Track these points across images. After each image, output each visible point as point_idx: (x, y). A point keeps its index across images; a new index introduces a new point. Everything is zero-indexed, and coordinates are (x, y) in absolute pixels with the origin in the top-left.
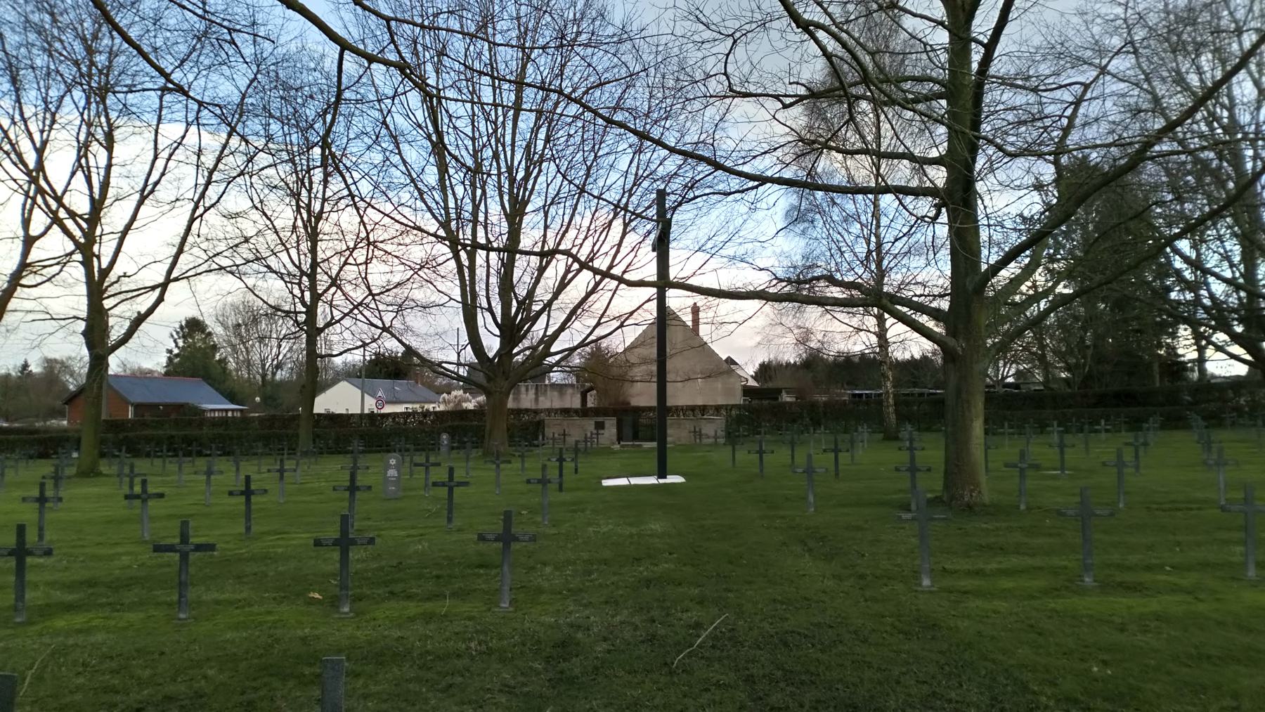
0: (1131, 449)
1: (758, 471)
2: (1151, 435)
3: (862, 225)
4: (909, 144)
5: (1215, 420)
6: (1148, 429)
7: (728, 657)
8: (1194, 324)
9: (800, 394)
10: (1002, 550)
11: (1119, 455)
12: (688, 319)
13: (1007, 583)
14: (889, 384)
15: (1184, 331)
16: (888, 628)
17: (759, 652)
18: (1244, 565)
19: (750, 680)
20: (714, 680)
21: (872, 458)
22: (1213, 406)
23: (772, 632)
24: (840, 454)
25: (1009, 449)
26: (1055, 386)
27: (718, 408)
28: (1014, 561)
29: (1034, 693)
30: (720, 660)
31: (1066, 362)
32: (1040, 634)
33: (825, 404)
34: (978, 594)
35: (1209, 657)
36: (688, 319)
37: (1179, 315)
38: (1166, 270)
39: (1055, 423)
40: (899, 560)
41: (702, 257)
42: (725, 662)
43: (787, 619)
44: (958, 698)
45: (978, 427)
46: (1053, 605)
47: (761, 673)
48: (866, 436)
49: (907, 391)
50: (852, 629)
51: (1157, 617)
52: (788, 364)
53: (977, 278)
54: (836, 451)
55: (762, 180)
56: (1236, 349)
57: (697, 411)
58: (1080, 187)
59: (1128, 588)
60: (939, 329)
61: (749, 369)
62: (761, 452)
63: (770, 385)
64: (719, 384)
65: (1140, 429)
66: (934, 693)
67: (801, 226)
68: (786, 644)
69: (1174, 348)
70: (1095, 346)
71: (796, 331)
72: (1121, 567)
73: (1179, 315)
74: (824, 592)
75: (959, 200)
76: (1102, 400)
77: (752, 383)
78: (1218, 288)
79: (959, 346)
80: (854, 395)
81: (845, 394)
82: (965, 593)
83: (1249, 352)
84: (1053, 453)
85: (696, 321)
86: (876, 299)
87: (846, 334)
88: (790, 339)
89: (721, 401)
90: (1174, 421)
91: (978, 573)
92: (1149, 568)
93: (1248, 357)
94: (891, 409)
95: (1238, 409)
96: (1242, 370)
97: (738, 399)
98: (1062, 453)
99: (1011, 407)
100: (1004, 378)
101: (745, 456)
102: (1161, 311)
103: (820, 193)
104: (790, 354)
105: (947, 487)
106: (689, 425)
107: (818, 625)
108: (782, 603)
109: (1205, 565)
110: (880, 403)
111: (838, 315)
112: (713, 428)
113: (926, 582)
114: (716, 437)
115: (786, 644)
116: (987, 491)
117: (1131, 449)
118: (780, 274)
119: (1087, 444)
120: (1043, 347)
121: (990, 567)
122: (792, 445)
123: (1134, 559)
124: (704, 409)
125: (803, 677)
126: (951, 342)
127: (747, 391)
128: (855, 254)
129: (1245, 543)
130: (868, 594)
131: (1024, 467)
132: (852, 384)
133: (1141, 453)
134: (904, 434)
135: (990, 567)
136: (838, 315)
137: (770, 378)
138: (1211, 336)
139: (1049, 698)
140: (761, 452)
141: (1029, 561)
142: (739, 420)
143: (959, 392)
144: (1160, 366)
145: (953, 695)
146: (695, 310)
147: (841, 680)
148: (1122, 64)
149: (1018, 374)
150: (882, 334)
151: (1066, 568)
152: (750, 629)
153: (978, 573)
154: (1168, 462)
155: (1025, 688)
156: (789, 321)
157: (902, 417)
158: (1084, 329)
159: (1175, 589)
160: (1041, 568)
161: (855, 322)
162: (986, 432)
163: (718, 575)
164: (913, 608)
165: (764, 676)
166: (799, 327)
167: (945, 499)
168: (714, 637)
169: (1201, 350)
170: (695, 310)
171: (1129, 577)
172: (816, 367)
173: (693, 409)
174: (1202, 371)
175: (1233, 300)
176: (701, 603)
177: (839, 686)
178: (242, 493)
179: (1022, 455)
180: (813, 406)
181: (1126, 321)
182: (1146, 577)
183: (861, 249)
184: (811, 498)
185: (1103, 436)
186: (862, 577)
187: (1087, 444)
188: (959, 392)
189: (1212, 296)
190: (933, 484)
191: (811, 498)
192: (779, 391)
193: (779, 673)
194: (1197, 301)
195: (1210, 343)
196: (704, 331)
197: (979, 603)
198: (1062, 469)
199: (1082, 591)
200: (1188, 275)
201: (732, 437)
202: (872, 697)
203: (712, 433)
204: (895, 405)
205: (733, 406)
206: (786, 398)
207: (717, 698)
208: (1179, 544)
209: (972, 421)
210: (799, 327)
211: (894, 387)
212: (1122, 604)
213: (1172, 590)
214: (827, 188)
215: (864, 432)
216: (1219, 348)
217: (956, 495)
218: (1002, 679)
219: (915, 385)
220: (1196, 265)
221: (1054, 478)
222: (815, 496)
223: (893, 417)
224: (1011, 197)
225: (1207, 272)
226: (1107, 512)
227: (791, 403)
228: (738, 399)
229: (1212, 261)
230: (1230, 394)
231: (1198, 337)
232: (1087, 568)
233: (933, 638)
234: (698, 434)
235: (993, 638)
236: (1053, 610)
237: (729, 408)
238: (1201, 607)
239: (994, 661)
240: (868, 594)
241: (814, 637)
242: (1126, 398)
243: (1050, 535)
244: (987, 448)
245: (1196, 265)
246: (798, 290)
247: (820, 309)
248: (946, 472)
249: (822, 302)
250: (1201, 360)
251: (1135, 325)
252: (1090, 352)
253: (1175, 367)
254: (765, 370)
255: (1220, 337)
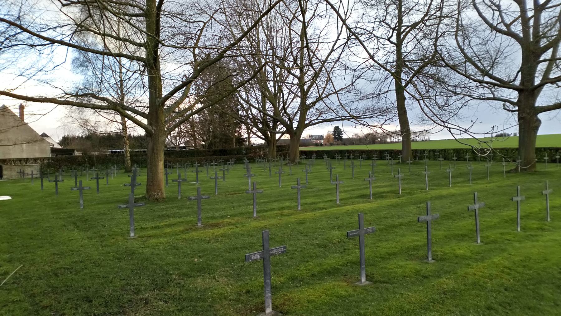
0: (222, 172)
1: (54, 190)
2: (231, 166)
3: (113, 71)
4: (465, 48)
5: (252, 160)
6: (229, 164)
7: (22, 287)
8: (246, 124)
9: (84, 152)
10: (169, 216)
11: (216, 174)
12: (16, 112)
13: (168, 230)
14: (127, 147)
15: (243, 126)
16: (111, 258)
17: (40, 281)
18: (253, 212)
19: (33, 296)
20: (11, 300)
21: (116, 181)
22: (251, 155)
23: (49, 269)
24: (100, 180)
25: (174, 174)
26: (198, 148)
27: (35, 160)
28: (172, 220)
29: (171, 274)
30: (16, 289)
31: (203, 138)
32: (177, 249)
33: (97, 157)
34: (155, 236)
35: (237, 248)
36: (16, 112)
37: (242, 121)
38: (237, 103)
39: (197, 163)
40: (122, 227)
41: (23, 79)
42: (20, 289)
43: (59, 262)
44: (138, 283)
45: (161, 165)
46: (184, 237)
47: (40, 291)
48: (116, 171)
49: (137, 150)
50: (92, 261)
51: (222, 236)
52: (78, 137)
53: (160, 100)
54: (97, 179)
55: (53, 41)
56: (259, 134)
57: (23, 161)
58: (203, 67)
59: (214, 226)
60: (145, 121)
61: (55, 140)
62: (56, 181)
63: (69, 147)
64: (37, 147)
65: (226, 164)
66: (127, 283)
67: (81, 68)
68: (56, 275)
69: (240, 133)
70: (213, 132)
71: (80, 121)
72: (213, 218)
73: (242, 121)
74: (82, 246)
75: (152, 64)
76: (215, 153)
77: (57, 146)
78: (254, 111)
79: (153, 130)
80: (112, 152)
81: (108, 152)
82: (149, 237)
83: (263, 135)
84: (194, 175)
85: (22, 114)
86: (119, 107)
87: (107, 123)
88: (76, 124)
89: (38, 155)
90: (239, 161)
91: (157, 227)
92: (222, 217)
93: (263, 137)
94: (128, 158)
95: (260, 156)
96: (263, 142)
97: (49, 155)
98: (197, 175)
99: (176, 157)
100: (179, 144)
101: (49, 184)
102: (236, 119)
103: (91, 53)
104: (79, 132)
105: (147, 192)
106: (17, 169)
107: (76, 262)
108: (58, 255)
109: (241, 214)
110: (123, 155)
111: (101, 114)
112: (33, 170)
113: (132, 234)
114: (32, 174)
115: (56, 275)
116: (165, 191)
117: (222, 172)
118: (69, 92)
119: (207, 170)
120: (194, 131)
121: (161, 224)
122: (76, 177)
123: (217, 214)
124: (27, 160)
125: (63, 289)
126: (150, 128)
127: (54, 150)
128: (109, 84)
129: (253, 205)
130: (104, 243)
131: (181, 181)
132: (112, 147)
133: (226, 173)
134: (133, 169)
135: (161, 224)
136: (101, 114)
137: (68, 144)
138: (252, 128)
139: (176, 275)
140: (56, 181)
141: (178, 220)
142: (49, 165)
143: (153, 149)
144: (236, 139)
145: (136, 283)
146: (22, 108)
147: (82, 286)
148: (220, 17)
149: (186, 143)
150: (124, 124)
151: (192, 221)
152: (37, 270)
153: (157, 227)
154: (233, 176)
155: (167, 273)
156: (76, 115)
157: (133, 162)
158: (209, 124)
159: (230, 224)
160: (182, 222)
161: (111, 117)
162: (165, 166)
163: (23, 246)
164: (124, 247)
165: (41, 292)
166: (81, 119)
167: (147, 197)
168: (15, 277)
169: (249, 134)
170: (22, 108)
171: (214, 222)
172: (93, 138)
173: (20, 160)
174: (249, 142)
175: (259, 116)
176: (10, 261)
177: (81, 290)
178: (96, 178)
179: (179, 176)
180: (90, 158)
181: (224, 122)
182: (220, 221)
183: (113, 81)
184: (81, 202)
185: (214, 167)
186: (103, 236)
187: (207, 170)
188: (153, 149)
189: (252, 114)
190: (141, 191)
191: (81, 202)
192: (73, 151)
193: (50, 289)
194: (247, 116)
195: (251, 131)
196: (26, 119)
197: (154, 240)
198: (197, 181)
199: (197, 229)
200: (245, 105)
201: (43, 174)
202: (97, 291)
203: (30, 173)
204: (130, 156)
205: (45, 158)
206: (77, 154)
207: (11, 309)
208: (234, 207)
209: (159, 162)
210: (81, 119)
211: (130, 148)
212: (211, 232)
213: (229, 225)
214: (94, 52)
215: (114, 169)
216: (255, 134)
217: (151, 196)
218: (158, 272)
219: (142, 147)
220: (247, 102)
221: (194, 185)
222: (83, 201)
223: (129, 162)
224: (175, 67)
225: (251, 105)
226: (206, 197)
227: (78, 156)
228: (49, 155)
229: (253, 101)
230: (258, 150)
231: (248, 129)
232: (199, 220)
233: (132, 259)
234: (22, 173)
235: (157, 254)
236: (185, 239)
237: (42, 159)
238: (237, 230)
239: (156, 265)
240: (104, 243)
241: (72, 268)
242: (223, 152)
243: (188, 208)
244: (166, 174)
245: (247, 102)
246: (81, 100)
247: (93, 110)
248: (147, 185)
249: (94, 107)
250: (249, 138)
251: (227, 124)
252: (211, 134)
253: (240, 140)
254: (65, 140)
255: (255, 129)
